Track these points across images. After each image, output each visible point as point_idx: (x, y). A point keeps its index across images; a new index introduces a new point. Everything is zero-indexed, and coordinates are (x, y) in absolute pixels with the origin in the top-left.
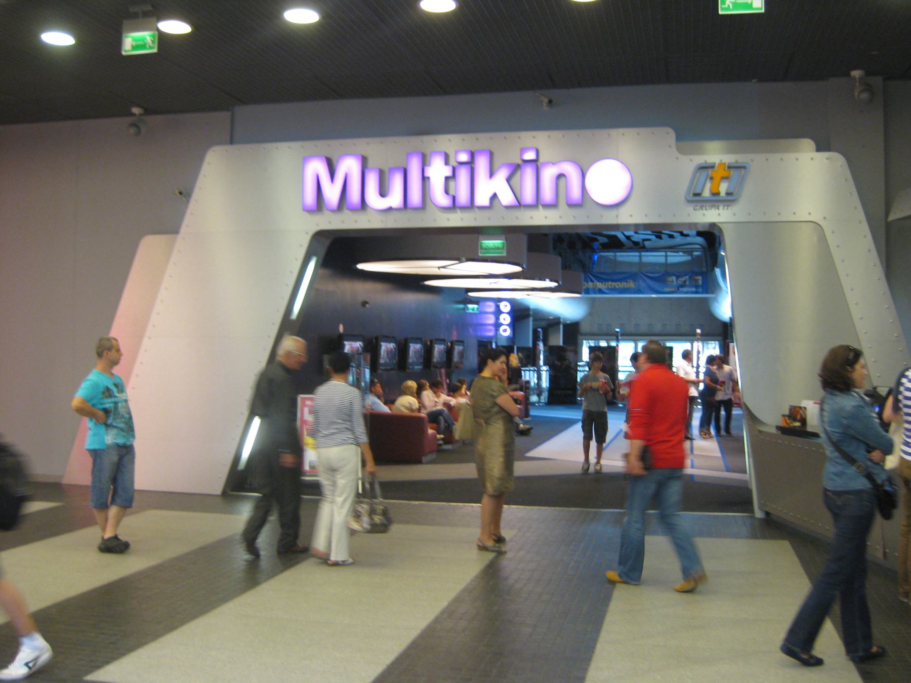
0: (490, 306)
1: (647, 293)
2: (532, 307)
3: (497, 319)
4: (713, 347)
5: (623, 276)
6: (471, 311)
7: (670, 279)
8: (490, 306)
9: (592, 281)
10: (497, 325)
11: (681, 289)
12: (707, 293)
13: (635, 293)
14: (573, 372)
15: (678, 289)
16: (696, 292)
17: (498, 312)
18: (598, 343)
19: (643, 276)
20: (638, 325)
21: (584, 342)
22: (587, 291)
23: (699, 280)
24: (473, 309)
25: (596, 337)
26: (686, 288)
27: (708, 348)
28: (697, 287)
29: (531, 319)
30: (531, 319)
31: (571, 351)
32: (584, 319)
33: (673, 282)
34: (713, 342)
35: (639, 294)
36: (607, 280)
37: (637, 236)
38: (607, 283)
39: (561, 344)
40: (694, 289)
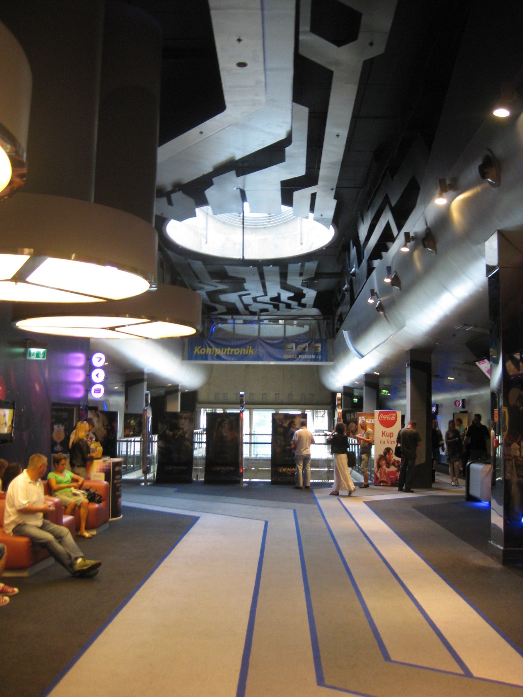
0: (79, 359)
1: (266, 360)
2: (146, 370)
3: (88, 375)
4: (322, 415)
5: (240, 342)
6: (34, 358)
7: (289, 346)
8: (79, 359)
9: (210, 347)
10: (89, 383)
11: (300, 356)
12: (327, 360)
13: (254, 360)
14: (187, 443)
15: (298, 356)
16: (315, 360)
17: (89, 368)
18: (305, 412)
19: (262, 343)
20: (252, 394)
21: (202, 409)
22: (205, 357)
23: (318, 347)
24: (38, 355)
25: (213, 405)
26: (306, 355)
27: (317, 416)
28: (316, 354)
29: (145, 384)
30: (145, 384)
31: (185, 418)
32: (201, 388)
33: (292, 348)
34: (321, 411)
35: (258, 360)
36: (227, 347)
37: (255, 304)
38: (226, 350)
39: (179, 410)
40: (313, 357)
